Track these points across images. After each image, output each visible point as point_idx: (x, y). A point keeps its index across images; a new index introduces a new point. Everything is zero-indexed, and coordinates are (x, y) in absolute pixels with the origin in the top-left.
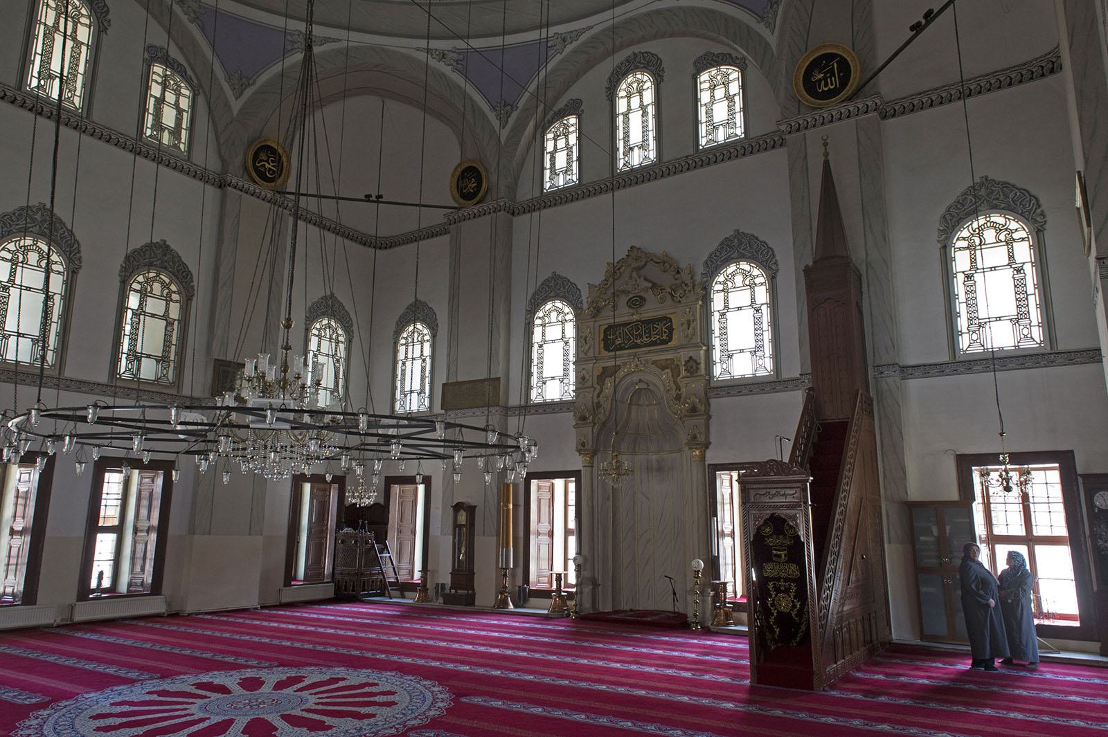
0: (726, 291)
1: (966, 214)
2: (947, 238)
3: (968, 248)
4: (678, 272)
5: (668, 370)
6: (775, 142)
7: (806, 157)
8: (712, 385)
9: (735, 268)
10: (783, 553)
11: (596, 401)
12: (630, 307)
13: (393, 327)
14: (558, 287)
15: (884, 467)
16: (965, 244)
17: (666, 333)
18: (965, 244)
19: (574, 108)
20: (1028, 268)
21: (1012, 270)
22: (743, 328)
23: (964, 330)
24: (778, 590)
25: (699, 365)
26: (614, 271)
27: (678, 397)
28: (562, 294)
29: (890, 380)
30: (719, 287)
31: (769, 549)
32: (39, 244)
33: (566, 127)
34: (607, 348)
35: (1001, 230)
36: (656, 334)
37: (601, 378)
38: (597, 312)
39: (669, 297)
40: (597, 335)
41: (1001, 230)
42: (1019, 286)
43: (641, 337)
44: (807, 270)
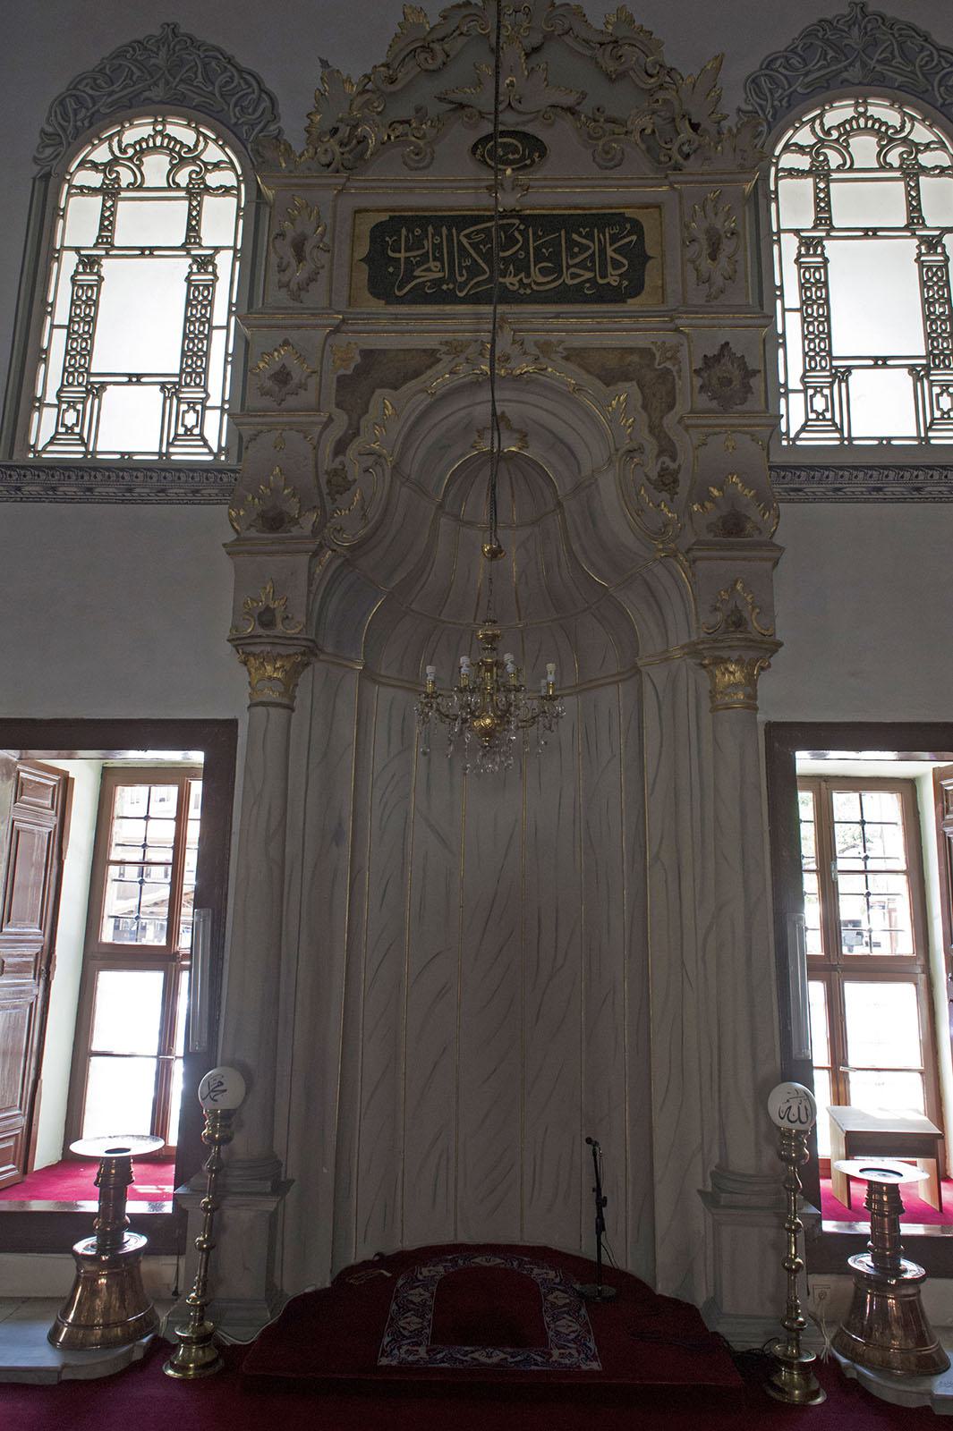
1: (111, 105)
5: (632, 387)
8: (776, 459)
11: (327, 463)
16: (95, 179)
17: (616, 264)
18: (95, 179)
20: (224, 261)
21: (916, 242)
23: (794, 383)
25: (743, 379)
27: (667, 481)
28: (198, 100)
32: (872, 111)
35: (891, 140)
36: (579, 265)
38: (350, 155)
41: (891, 140)
43: (522, 267)
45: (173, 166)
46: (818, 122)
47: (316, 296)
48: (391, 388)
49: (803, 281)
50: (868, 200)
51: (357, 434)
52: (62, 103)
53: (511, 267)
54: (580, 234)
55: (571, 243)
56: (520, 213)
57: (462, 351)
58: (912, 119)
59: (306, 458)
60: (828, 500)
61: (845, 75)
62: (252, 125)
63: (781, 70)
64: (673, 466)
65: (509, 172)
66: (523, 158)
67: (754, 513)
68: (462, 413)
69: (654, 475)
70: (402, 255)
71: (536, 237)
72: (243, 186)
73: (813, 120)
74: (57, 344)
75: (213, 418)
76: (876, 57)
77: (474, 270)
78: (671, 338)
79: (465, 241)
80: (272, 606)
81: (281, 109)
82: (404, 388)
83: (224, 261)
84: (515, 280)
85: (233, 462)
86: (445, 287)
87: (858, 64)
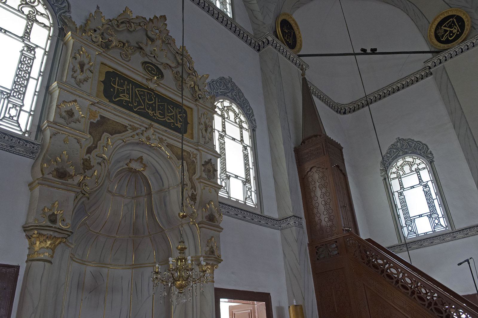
0: (399, 177)
3: (397, 177)
9: (402, 162)
13: (379, 167)
16: (395, 175)
18: (395, 175)
20: (430, 184)
21: (422, 186)
28: (410, 152)
30: (395, 176)
35: (412, 165)
41: (412, 165)
42: (427, 194)
43: (154, 109)
45: (410, 167)
46: (396, 166)
47: (86, 86)
48: (110, 134)
49: (14, 88)
50: (411, 180)
51: (96, 147)
53: (151, 108)
54: (170, 106)
55: (168, 109)
56: (154, 91)
57: (135, 130)
58: (241, 113)
59: (77, 151)
61: (228, 94)
62: (60, 9)
65: (156, 78)
67: (217, 216)
68: (128, 152)
70: (116, 87)
73: (395, 165)
74: (401, 212)
75: (442, 220)
76: (404, 148)
77: (139, 104)
78: (195, 152)
79: (137, 92)
80: (56, 213)
82: (114, 136)
83: (430, 184)
85: (33, 139)
86: (130, 105)
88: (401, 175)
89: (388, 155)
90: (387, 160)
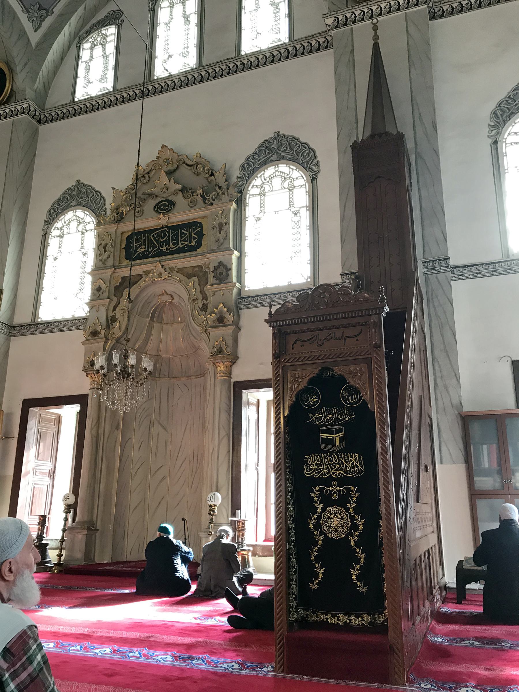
0: (262, 194)
2: (498, 133)
4: (212, 174)
5: (196, 279)
6: (320, 44)
7: (352, 51)
10: (337, 437)
12: (157, 212)
14: (81, 196)
15: (435, 374)
17: (194, 238)
19: (115, 18)
22: (281, 240)
24: (327, 501)
26: (142, 177)
27: (204, 308)
28: (84, 203)
29: (441, 276)
30: (256, 191)
31: (315, 430)
33: (105, 36)
34: (128, 257)
37: (118, 290)
38: (119, 218)
39: (200, 199)
40: (118, 241)
43: (167, 243)
44: (356, 148)
45: (283, 181)
51: (119, 303)
52: (50, 211)
55: (182, 233)
60: (258, 307)
61: (271, 158)
63: (252, 160)
64: (206, 303)
66: (169, 208)
69: (201, 307)
71: (172, 233)
72: (307, 184)
73: (261, 176)
76: (282, 150)
79: (152, 237)
81: (317, 154)
84: (165, 248)
87: (275, 154)
88: (266, 191)
89: (510, 101)
90: (506, 109)
